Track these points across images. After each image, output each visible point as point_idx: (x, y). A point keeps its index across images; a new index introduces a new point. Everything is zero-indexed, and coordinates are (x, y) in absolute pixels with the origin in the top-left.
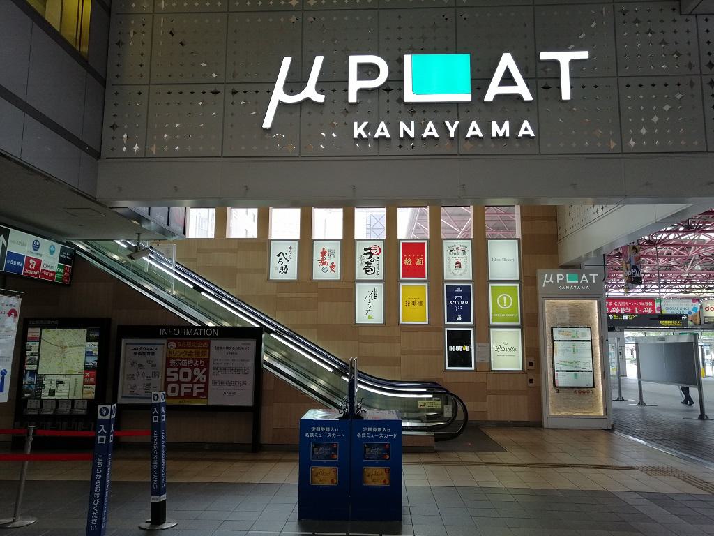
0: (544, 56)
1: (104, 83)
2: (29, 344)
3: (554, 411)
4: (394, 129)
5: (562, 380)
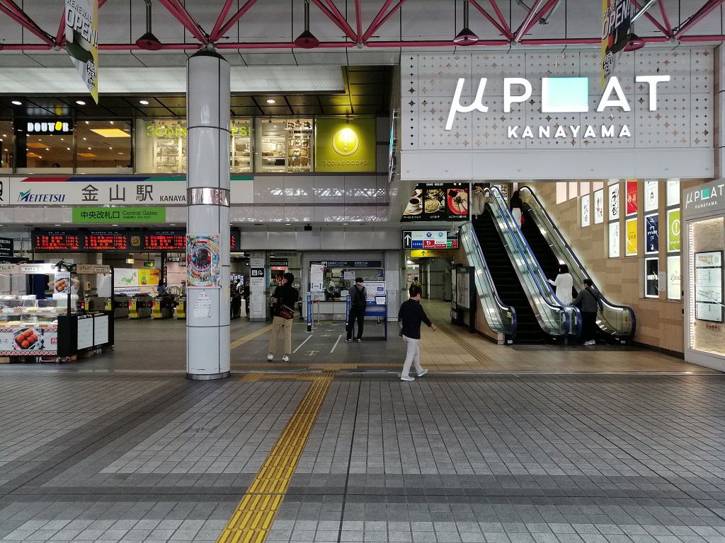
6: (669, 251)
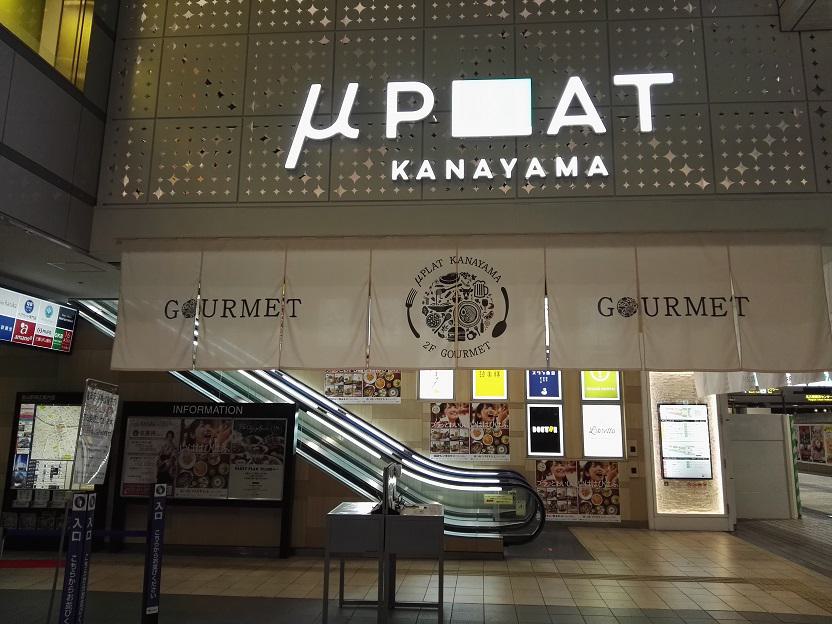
0: (619, 80)
1: (102, 116)
2: (22, 423)
3: (664, 506)
4: (439, 169)
5: (673, 470)
6: (584, 398)
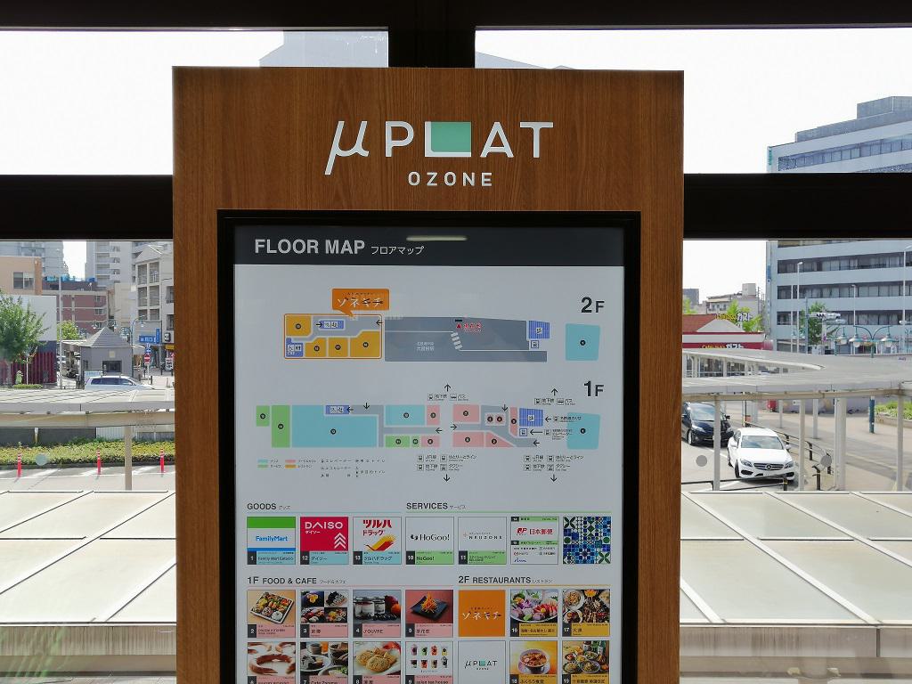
0: (523, 125)
